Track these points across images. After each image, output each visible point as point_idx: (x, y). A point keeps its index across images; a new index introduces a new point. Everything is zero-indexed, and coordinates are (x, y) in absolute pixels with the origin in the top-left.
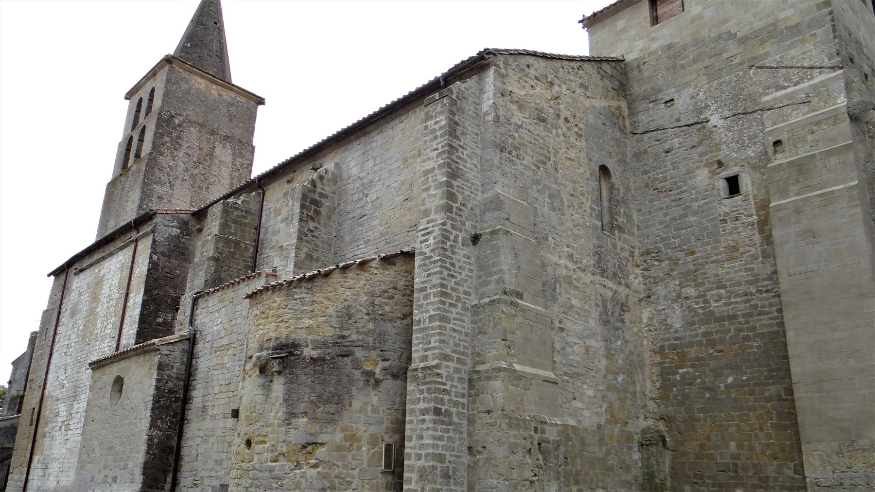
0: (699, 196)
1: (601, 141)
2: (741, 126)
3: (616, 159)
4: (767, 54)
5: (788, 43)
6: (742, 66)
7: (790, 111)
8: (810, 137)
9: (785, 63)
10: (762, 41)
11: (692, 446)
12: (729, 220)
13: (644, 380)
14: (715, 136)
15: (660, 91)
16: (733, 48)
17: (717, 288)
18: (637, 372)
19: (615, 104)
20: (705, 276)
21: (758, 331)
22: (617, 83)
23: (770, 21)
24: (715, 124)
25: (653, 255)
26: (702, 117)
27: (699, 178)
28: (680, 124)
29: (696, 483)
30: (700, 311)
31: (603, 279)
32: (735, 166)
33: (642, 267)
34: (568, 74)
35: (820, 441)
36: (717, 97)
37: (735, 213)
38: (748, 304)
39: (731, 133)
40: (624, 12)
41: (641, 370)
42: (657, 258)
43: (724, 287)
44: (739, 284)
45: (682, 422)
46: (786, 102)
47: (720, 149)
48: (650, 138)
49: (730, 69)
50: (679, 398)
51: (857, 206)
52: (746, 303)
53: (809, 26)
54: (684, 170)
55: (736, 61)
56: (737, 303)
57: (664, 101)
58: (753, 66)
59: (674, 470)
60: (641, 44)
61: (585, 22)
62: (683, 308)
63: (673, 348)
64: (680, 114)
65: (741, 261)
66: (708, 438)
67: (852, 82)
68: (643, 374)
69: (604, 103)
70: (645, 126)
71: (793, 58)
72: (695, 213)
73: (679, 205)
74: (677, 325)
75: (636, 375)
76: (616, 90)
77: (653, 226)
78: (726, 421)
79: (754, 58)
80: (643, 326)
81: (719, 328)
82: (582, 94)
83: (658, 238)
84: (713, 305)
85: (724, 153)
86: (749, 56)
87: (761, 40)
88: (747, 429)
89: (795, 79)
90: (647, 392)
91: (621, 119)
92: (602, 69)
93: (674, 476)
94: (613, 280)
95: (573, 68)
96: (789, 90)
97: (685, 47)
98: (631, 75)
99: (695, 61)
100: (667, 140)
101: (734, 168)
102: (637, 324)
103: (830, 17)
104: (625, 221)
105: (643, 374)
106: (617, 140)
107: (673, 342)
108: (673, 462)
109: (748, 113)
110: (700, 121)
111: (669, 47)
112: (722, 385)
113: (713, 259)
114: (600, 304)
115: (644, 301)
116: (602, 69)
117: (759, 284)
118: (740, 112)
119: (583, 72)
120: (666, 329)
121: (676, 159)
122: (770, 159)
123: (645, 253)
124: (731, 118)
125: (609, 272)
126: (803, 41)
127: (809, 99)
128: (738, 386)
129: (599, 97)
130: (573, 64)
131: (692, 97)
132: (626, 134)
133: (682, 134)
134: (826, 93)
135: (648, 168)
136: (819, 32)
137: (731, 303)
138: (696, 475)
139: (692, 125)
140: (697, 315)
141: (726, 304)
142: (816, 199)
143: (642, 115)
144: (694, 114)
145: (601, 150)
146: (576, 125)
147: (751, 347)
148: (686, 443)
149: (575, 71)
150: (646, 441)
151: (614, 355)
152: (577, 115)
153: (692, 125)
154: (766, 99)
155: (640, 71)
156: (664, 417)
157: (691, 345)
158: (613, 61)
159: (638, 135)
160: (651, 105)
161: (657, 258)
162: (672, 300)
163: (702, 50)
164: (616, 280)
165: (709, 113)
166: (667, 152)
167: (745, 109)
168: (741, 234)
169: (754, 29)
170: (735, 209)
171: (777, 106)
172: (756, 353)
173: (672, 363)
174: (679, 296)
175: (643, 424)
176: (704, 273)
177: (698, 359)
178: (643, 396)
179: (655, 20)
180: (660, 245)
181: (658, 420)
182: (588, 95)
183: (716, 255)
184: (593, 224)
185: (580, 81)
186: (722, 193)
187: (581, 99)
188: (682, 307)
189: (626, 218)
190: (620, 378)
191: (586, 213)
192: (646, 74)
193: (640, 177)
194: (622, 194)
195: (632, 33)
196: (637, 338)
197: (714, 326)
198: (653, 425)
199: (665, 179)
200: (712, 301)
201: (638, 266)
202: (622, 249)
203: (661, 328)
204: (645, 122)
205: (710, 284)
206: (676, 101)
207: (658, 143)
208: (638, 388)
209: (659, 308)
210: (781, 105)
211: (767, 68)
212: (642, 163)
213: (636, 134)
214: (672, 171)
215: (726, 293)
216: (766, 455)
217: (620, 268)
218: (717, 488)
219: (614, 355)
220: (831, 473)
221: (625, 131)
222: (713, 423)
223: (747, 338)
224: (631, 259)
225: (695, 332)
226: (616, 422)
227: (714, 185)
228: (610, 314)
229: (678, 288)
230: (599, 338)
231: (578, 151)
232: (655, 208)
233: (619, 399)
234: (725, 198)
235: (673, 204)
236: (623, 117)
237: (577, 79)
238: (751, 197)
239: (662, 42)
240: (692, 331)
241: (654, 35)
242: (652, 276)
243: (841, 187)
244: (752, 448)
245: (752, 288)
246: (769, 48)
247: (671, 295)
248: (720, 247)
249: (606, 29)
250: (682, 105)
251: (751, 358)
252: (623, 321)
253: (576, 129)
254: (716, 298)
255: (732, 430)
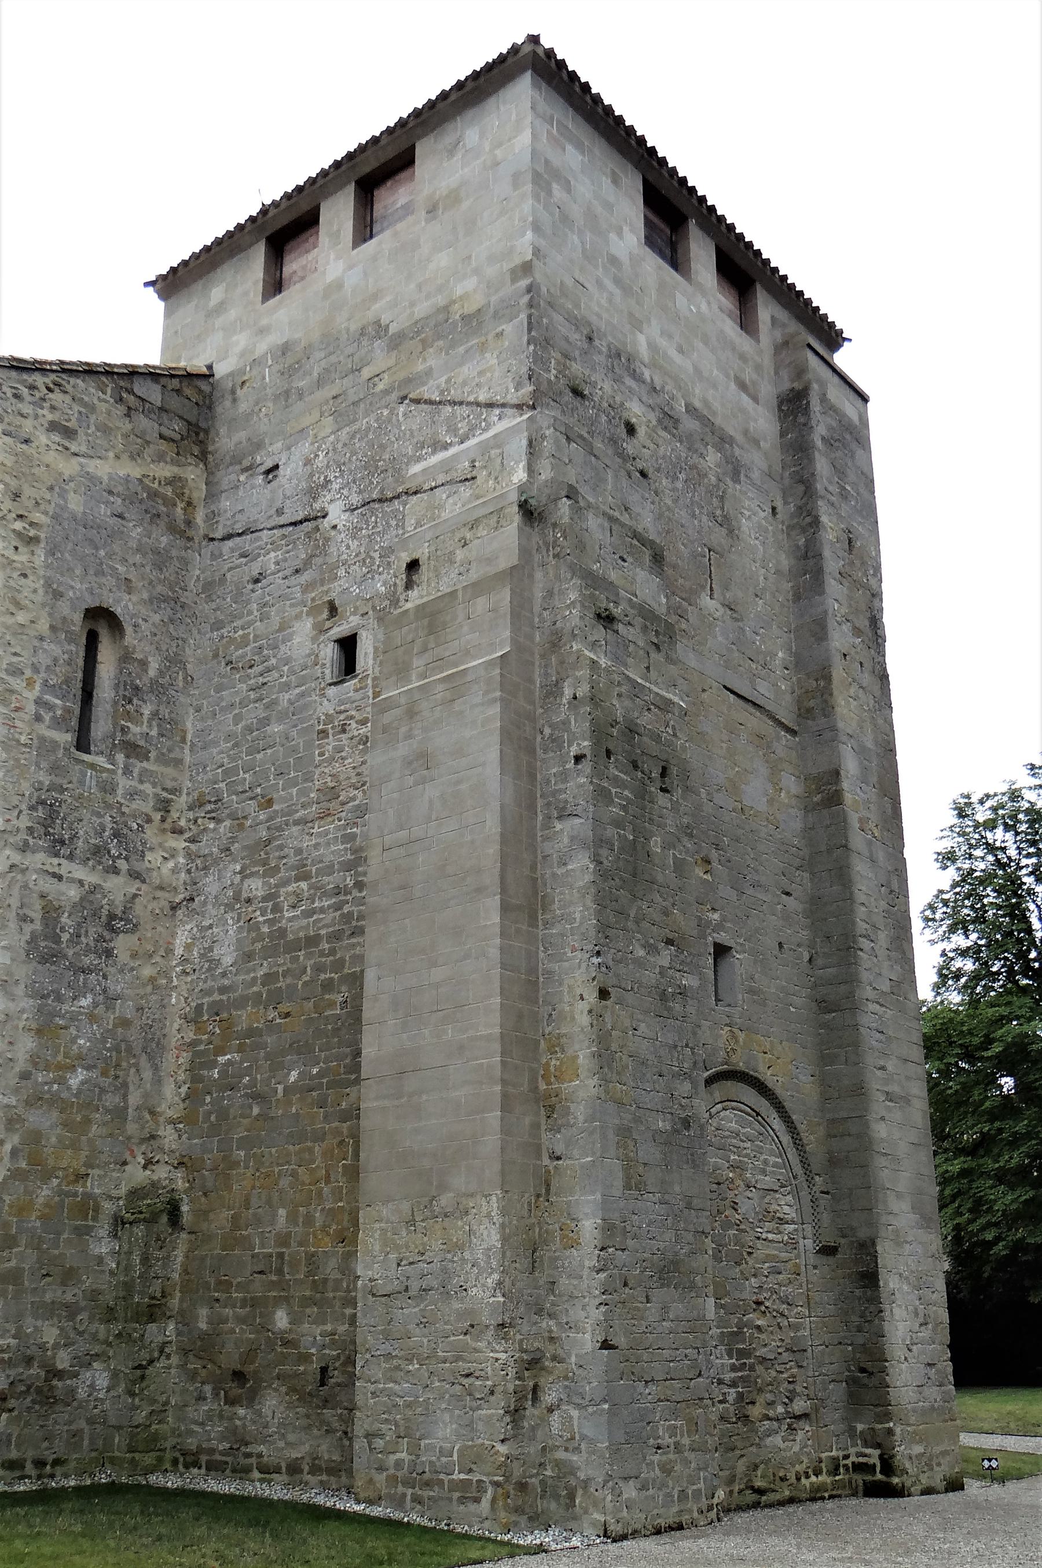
0: (293, 678)
1: (102, 553)
2: (373, 528)
3: (145, 596)
4: (429, 373)
5: (461, 349)
6: (388, 398)
7: (444, 496)
8: (460, 555)
9: (454, 394)
10: (425, 344)
11: (221, 1219)
12: (331, 731)
13: (158, 1082)
14: (333, 550)
15: (259, 446)
16: (381, 359)
17: (298, 879)
18: (136, 1065)
19: (165, 471)
20: (282, 854)
21: (346, 971)
22: (177, 425)
23: (440, 300)
24: (334, 522)
25: (209, 807)
26: (317, 506)
27: (297, 640)
28: (283, 520)
29: (217, 1300)
30: (265, 929)
31: (56, 861)
32: (354, 613)
33: (187, 835)
34: (14, 401)
35: (386, 1202)
36: (344, 464)
37: (342, 717)
38: (339, 912)
39: (356, 543)
40: (225, 266)
41: (151, 1058)
42: (213, 815)
43: (305, 877)
44: (329, 870)
45: (211, 1170)
46: (441, 478)
47: (336, 578)
48: (232, 550)
49: (371, 404)
50: (213, 1118)
51: (494, 700)
52: (336, 910)
53: (496, 315)
54: (275, 621)
55: (381, 386)
56: (322, 910)
57: (263, 468)
58: (405, 398)
59: (188, 1273)
60: (241, 340)
61: (158, 286)
62: (241, 923)
63: (216, 1009)
64: (285, 497)
65: (340, 820)
66: (247, 1205)
67: (543, 437)
68: (156, 1068)
69: (132, 470)
70: (229, 523)
71: (465, 383)
72: (282, 717)
73: (259, 699)
74: (228, 960)
75: (133, 1070)
76: (173, 441)
77: (215, 743)
78: (278, 1165)
79: (408, 381)
80: (174, 963)
81: (289, 965)
82: (54, 447)
83: (220, 771)
84: (287, 915)
85: (340, 586)
86: (402, 375)
87: (423, 341)
88: (306, 1179)
89: (463, 427)
90: (162, 1108)
91: (180, 505)
92: (130, 392)
93: (186, 1288)
94: (91, 863)
95: (32, 387)
96: (452, 451)
97: (308, 352)
98: (219, 409)
99: (320, 383)
100: (259, 555)
101: (352, 618)
102: (157, 959)
103: (526, 299)
104: (154, 733)
105: (156, 1068)
106: (156, 552)
107: (216, 997)
108: (187, 1257)
109: (387, 500)
110: (313, 515)
111: (285, 349)
112: (280, 1088)
113: (297, 816)
114: (37, 916)
115: (184, 909)
116: (130, 392)
117: (360, 869)
118: (374, 496)
119: (68, 399)
120: (209, 969)
121: (268, 598)
122: (398, 601)
123: (197, 804)
124: (360, 511)
125: (80, 844)
126: (483, 348)
127: (474, 473)
128: (304, 1089)
129: (111, 454)
130: (39, 379)
131: (308, 462)
132: (190, 539)
133: (283, 542)
134: (499, 460)
135: (222, 617)
136: (508, 328)
137: (314, 912)
138: (219, 1283)
139: (301, 522)
140: (260, 938)
141: (309, 913)
142: (440, 687)
143: (227, 499)
144: (305, 499)
145: (99, 573)
146: (20, 516)
147: (332, 1004)
148: (212, 1216)
149: (38, 395)
150: (133, 1214)
151: (66, 1028)
152: (27, 492)
153: (301, 522)
154: (416, 468)
155: (235, 400)
156: (185, 1160)
157: (241, 1003)
158: (172, 376)
159: (216, 543)
160: (242, 478)
161: (213, 815)
162: (226, 905)
163: (333, 359)
164: (100, 863)
165: (328, 498)
166: (257, 581)
167: (382, 491)
168: (346, 762)
169: (417, 317)
170: (342, 708)
171: (426, 487)
172: (338, 1017)
173: (210, 1043)
174: (237, 897)
175: (137, 1175)
176: (281, 847)
177: (251, 1032)
178: (148, 1117)
179: (275, 285)
180: (221, 785)
181: (176, 1168)
182: (74, 448)
183: (304, 806)
184: (42, 739)
185: (50, 417)
186: (328, 672)
187: (51, 457)
188: (239, 921)
189: (159, 726)
190: (76, 1079)
191: (21, 714)
192: (243, 407)
193: (208, 636)
194: (152, 673)
195: (233, 314)
196: (149, 989)
197: (283, 962)
198: (166, 1178)
199: (244, 642)
200: (286, 908)
201: (178, 831)
202: (132, 794)
203: (202, 967)
204: (229, 514)
205: (287, 870)
206: (281, 471)
207: (243, 560)
208: (134, 1099)
209: (204, 923)
210: (433, 484)
211: (426, 402)
212: (214, 605)
213: (212, 539)
214: (258, 623)
215: (309, 889)
216: (328, 1234)
217: (116, 834)
218: (248, 1309)
219: (66, 1028)
220: (395, 1265)
221: (190, 533)
222: (258, 1170)
223: (328, 986)
224: (157, 817)
225: (252, 975)
226: (47, 1176)
227: (317, 655)
228: (65, 937)
229: (237, 879)
230: (20, 990)
231: (15, 575)
232: (224, 704)
233: (65, 1125)
234: (330, 685)
235: (252, 695)
236: (189, 504)
237: (45, 412)
238: (369, 681)
239: (275, 339)
240: (248, 972)
241: (264, 322)
242: (202, 853)
243: (480, 661)
244: (309, 1220)
245: (348, 879)
246: (433, 360)
247: (225, 895)
248: (311, 790)
249: (193, 304)
250: (290, 480)
251: (330, 1027)
252: (109, 953)
253: (18, 525)
254: (292, 900)
255: (284, 1182)
